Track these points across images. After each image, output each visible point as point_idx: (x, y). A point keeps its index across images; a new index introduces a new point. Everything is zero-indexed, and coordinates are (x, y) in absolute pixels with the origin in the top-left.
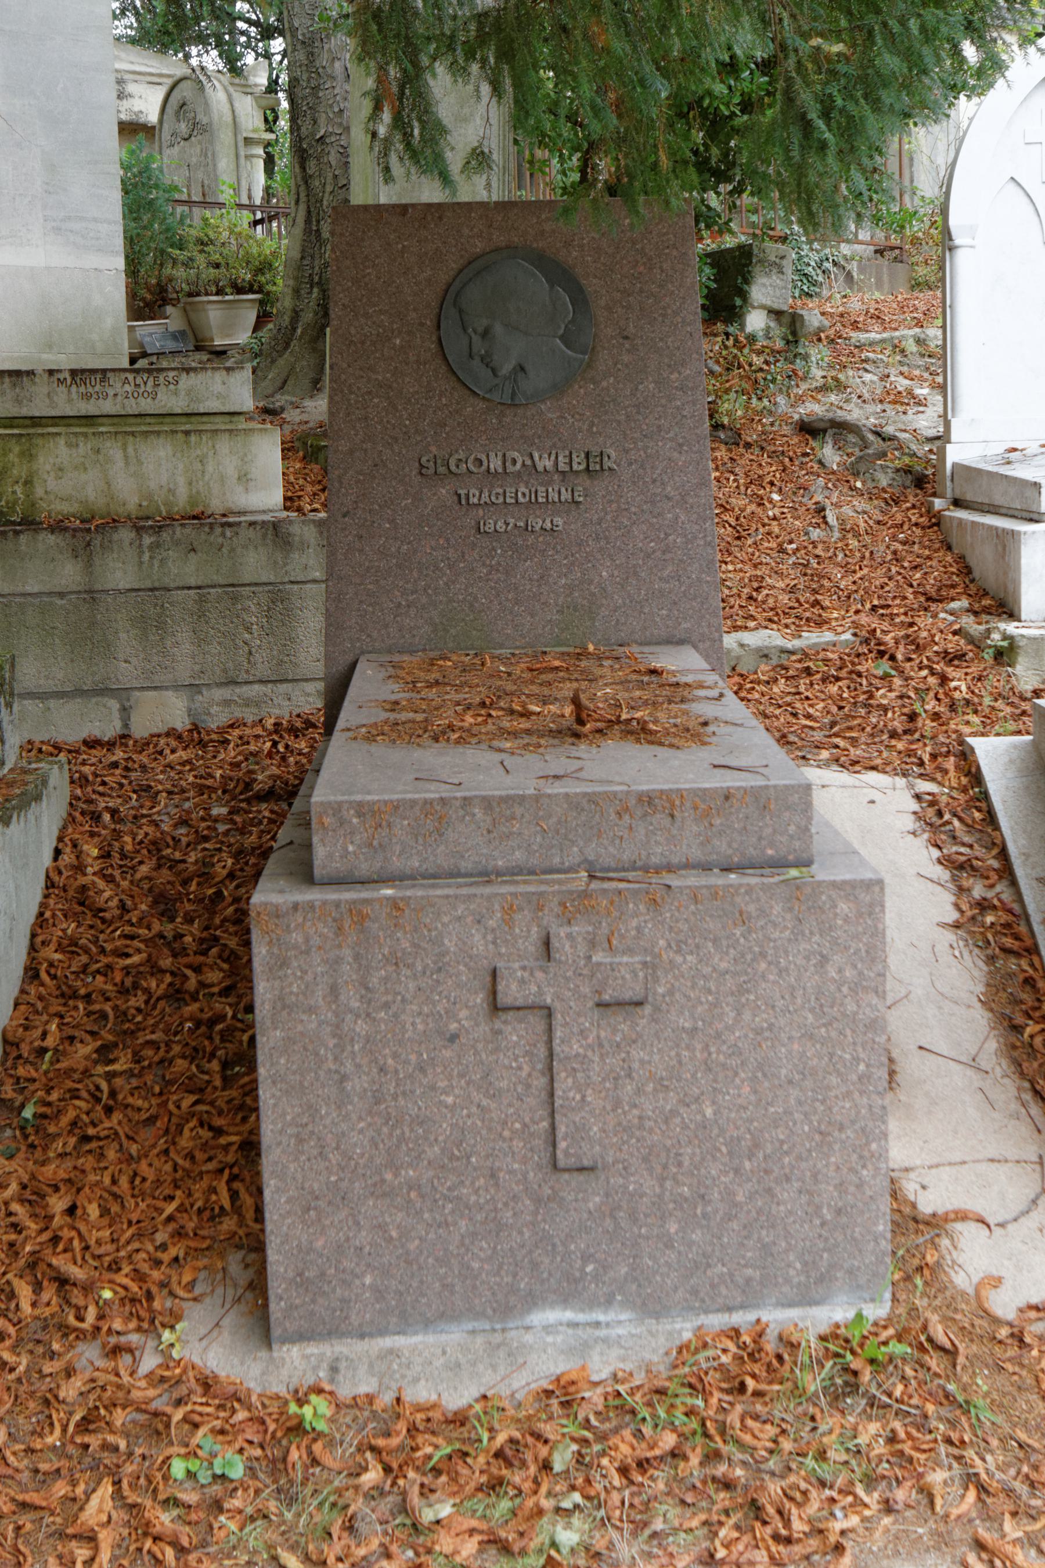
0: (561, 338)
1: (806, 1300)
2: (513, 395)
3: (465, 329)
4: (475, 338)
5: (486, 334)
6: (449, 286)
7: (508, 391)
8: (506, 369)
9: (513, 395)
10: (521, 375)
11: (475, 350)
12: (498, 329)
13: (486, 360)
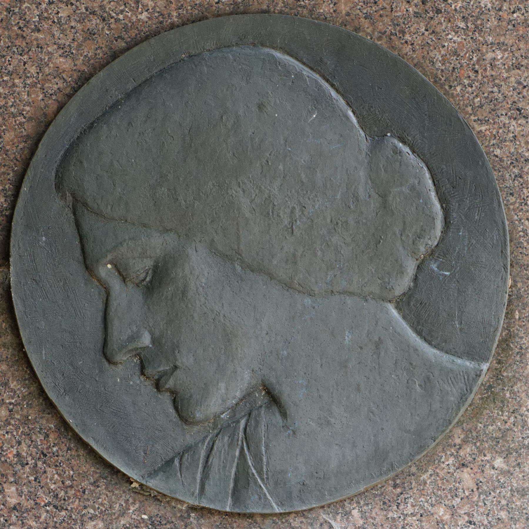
0: (403, 303)
1: (491, 351)
2: (242, 482)
3: (88, 265)
4: (123, 296)
5: (157, 281)
6: (44, 124)
7: (224, 469)
8: (219, 399)
9: (242, 482)
10: (268, 418)
11: (119, 332)
12: (199, 267)
13: (155, 368)
